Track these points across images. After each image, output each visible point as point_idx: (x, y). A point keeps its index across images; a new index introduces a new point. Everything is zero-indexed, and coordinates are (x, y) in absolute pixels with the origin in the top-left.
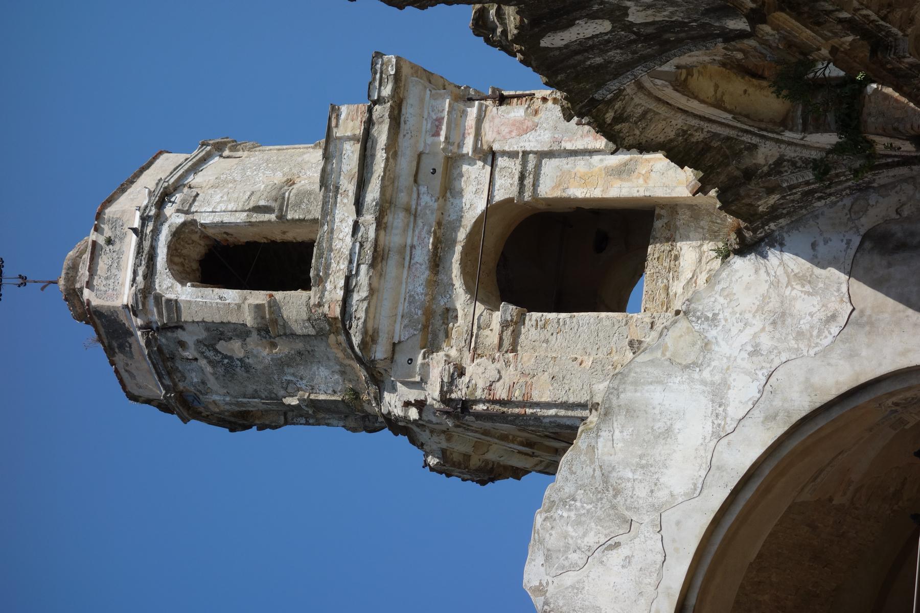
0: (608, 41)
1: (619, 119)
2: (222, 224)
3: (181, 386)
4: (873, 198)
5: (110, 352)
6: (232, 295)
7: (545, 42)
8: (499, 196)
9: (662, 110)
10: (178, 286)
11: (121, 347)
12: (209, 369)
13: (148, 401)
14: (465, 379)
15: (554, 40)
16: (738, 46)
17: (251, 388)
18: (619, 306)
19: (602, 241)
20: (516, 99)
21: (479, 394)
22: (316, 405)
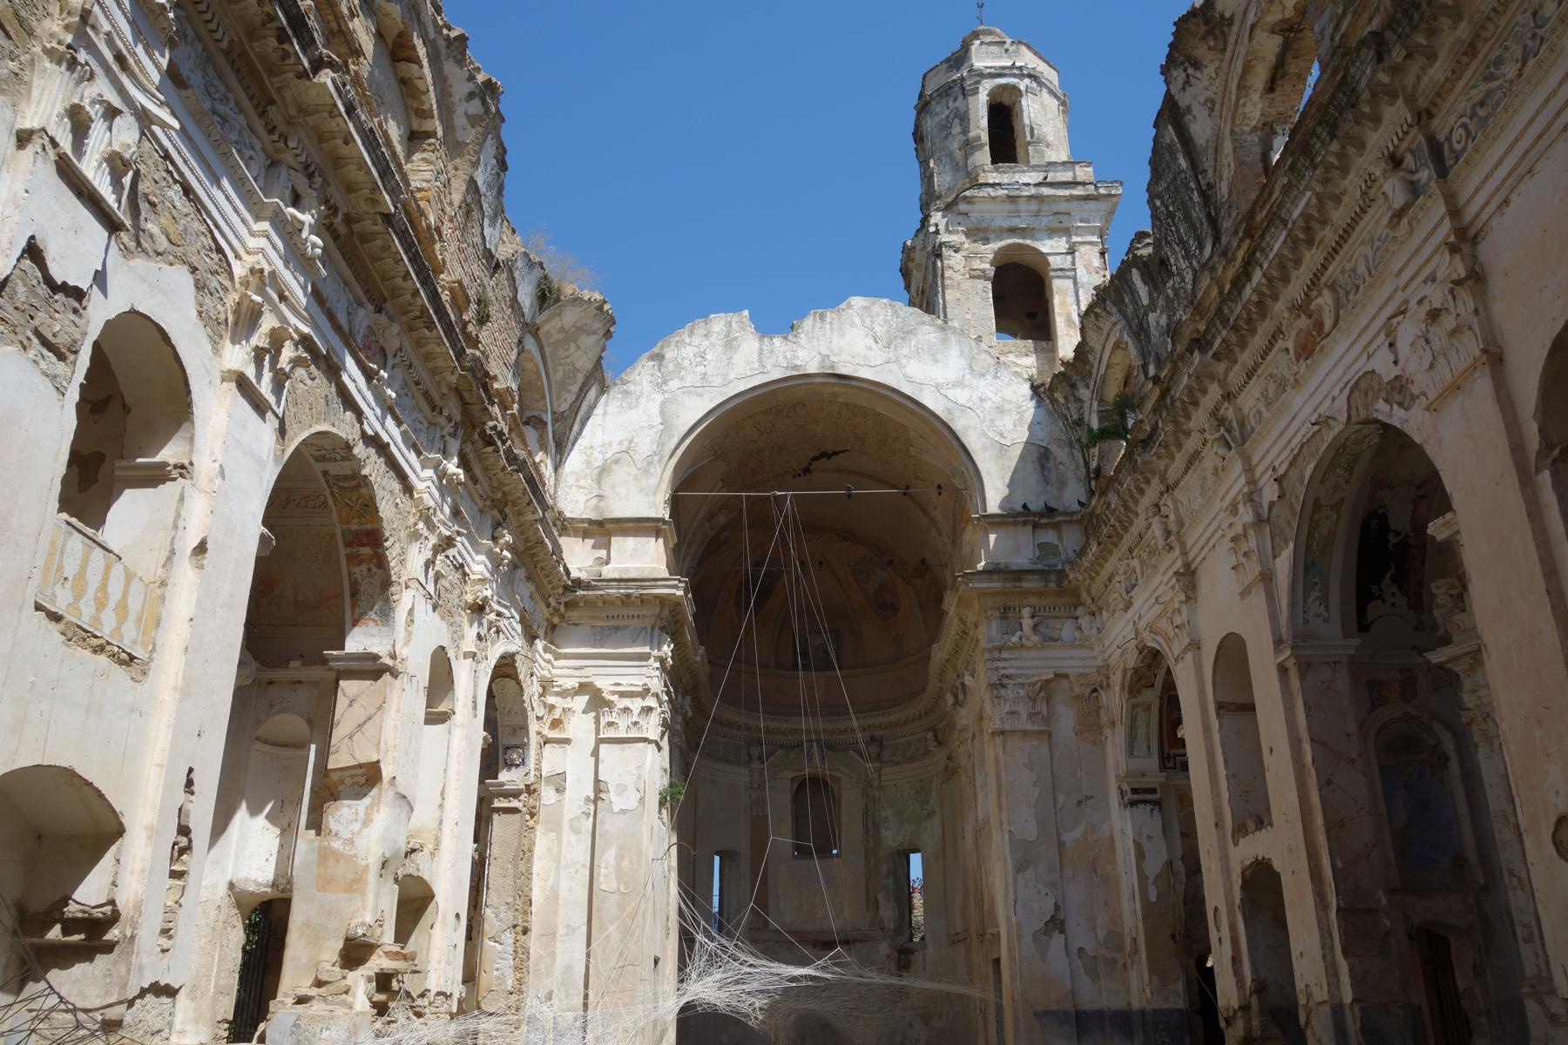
0: (1137, 304)
1: (1097, 315)
2: (1022, 112)
3: (933, 102)
4: (1066, 450)
5: (948, 60)
6: (984, 122)
7: (1134, 271)
8: (1050, 259)
9: (1104, 337)
10: (986, 93)
11: (950, 67)
12: (944, 116)
13: (923, 86)
14: (953, 254)
15: (1136, 276)
16: (552, 491)
18: (999, 329)
19: (1032, 316)
21: (946, 262)
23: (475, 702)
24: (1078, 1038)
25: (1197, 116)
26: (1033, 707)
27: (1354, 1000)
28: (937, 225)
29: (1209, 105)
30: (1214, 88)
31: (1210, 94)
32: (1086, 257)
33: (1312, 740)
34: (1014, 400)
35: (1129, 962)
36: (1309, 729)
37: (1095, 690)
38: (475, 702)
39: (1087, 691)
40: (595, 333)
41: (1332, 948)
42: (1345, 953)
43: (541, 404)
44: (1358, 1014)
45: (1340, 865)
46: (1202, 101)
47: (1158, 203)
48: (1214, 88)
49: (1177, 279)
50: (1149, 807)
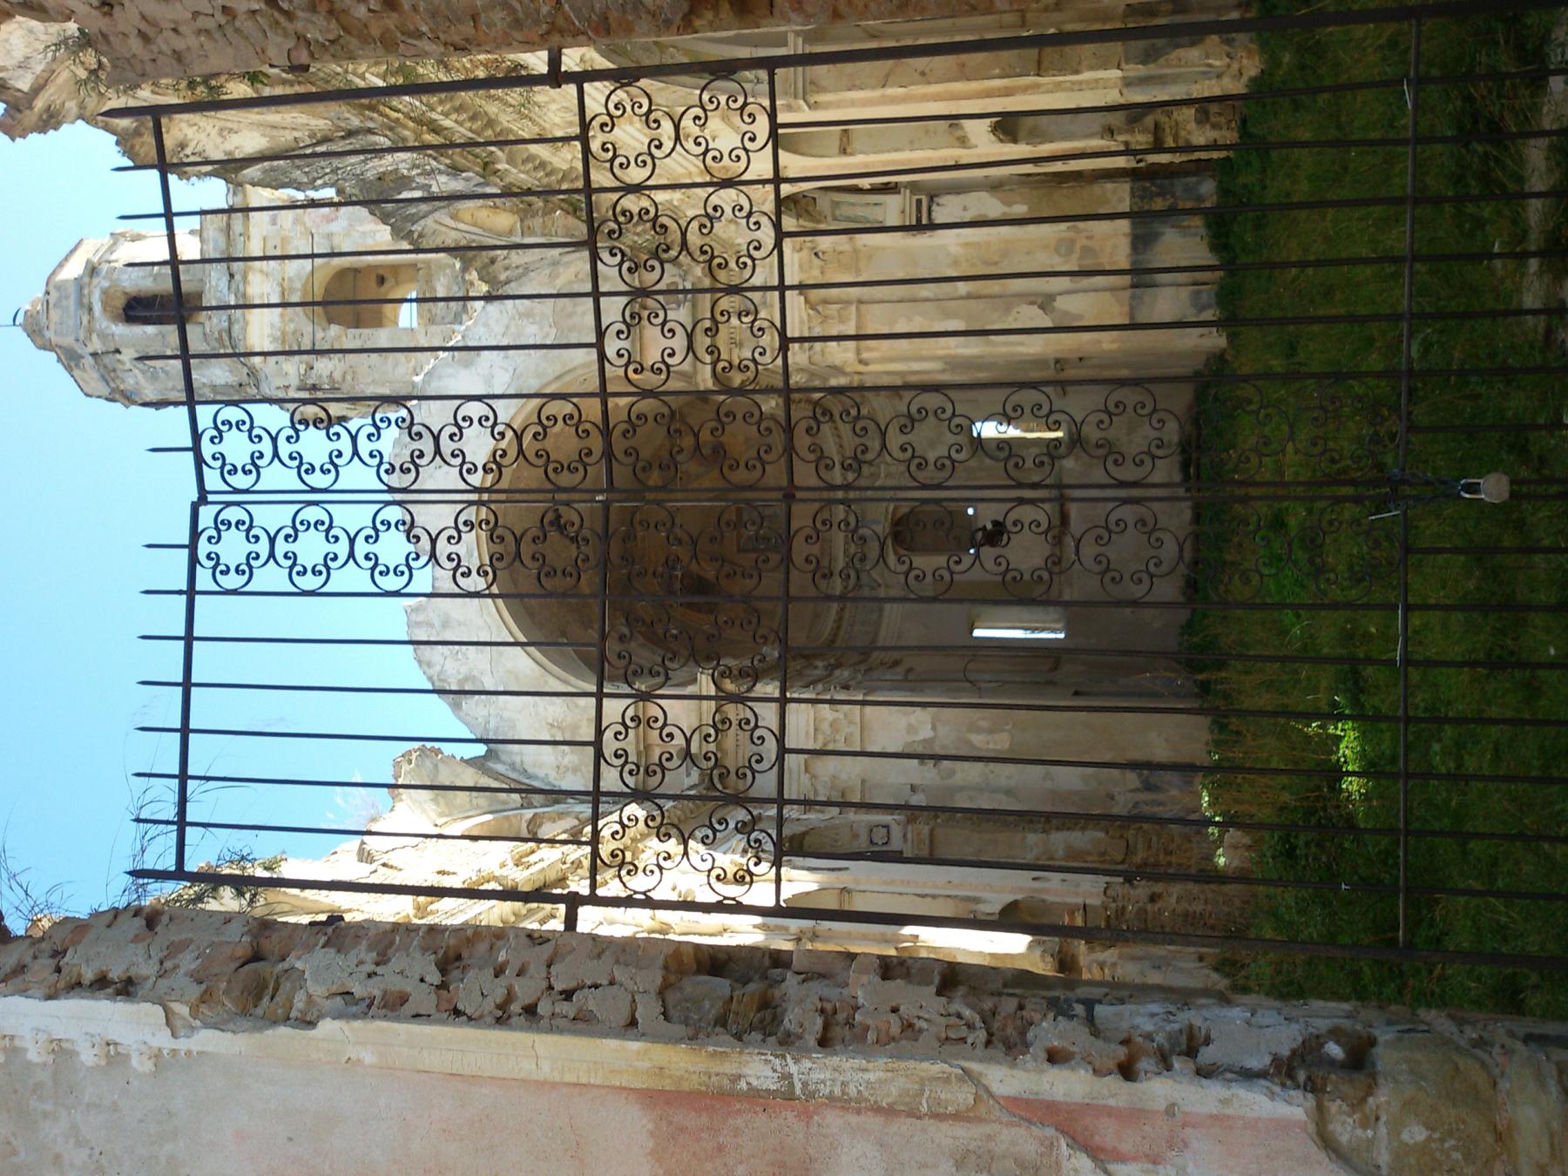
3: (122, 387)
4: (561, 270)
5: (69, 369)
9: (444, 229)
10: (113, 327)
11: (77, 365)
12: (140, 376)
13: (99, 397)
14: (314, 371)
17: (170, 384)
20: (1201, 774)
22: (1484, 776)
23: (833, 870)
24: (1156, 286)
25: (237, 144)
26: (832, 318)
27: (1119, 67)
28: (278, 388)
29: (225, 133)
30: (209, 128)
31: (214, 132)
32: (318, 220)
33: (883, 86)
34: (506, 321)
35: (1085, 234)
36: (873, 88)
37: (816, 254)
38: (833, 870)
39: (816, 261)
40: (436, 766)
41: (1073, 83)
42: (1077, 72)
43: (514, 820)
44: (1131, 66)
45: (997, 71)
46: (219, 140)
47: (319, 182)
48: (209, 128)
49: (400, 166)
50: (934, 207)
